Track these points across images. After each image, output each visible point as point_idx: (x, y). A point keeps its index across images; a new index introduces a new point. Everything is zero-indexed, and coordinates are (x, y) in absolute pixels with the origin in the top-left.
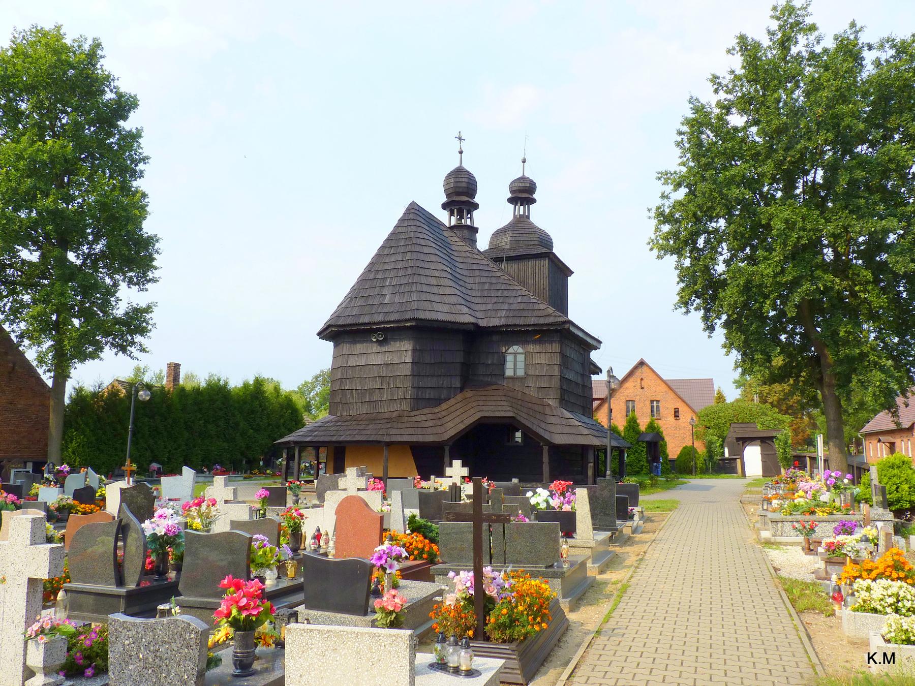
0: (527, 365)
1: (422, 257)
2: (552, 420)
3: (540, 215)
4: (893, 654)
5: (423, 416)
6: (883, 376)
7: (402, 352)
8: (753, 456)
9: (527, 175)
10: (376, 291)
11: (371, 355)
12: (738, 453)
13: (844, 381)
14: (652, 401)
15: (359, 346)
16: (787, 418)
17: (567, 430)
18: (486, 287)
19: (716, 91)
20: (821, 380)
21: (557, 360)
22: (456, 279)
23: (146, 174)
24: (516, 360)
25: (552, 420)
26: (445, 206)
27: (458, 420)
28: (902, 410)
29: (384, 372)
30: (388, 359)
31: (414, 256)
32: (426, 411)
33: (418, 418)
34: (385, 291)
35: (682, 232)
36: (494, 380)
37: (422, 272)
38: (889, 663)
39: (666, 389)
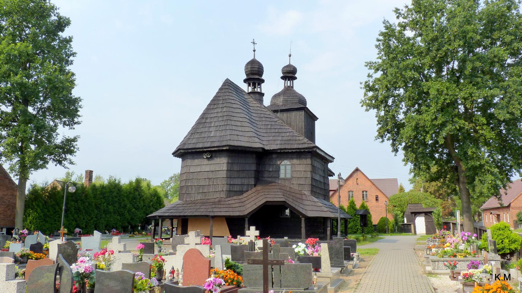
0: (292, 171)
1: (233, 110)
2: (307, 203)
3: (299, 86)
5: (234, 201)
6: (493, 178)
8: (420, 222)
9: (292, 63)
10: (206, 130)
11: (202, 165)
13: (471, 180)
14: (363, 192)
16: (439, 201)
18: (269, 127)
19: (398, 17)
20: (458, 180)
24: (286, 168)
25: (307, 203)
26: (245, 81)
28: (504, 197)
30: (213, 168)
31: (228, 109)
32: (235, 198)
33: (230, 202)
35: (378, 97)
37: (232, 118)
39: (371, 184)
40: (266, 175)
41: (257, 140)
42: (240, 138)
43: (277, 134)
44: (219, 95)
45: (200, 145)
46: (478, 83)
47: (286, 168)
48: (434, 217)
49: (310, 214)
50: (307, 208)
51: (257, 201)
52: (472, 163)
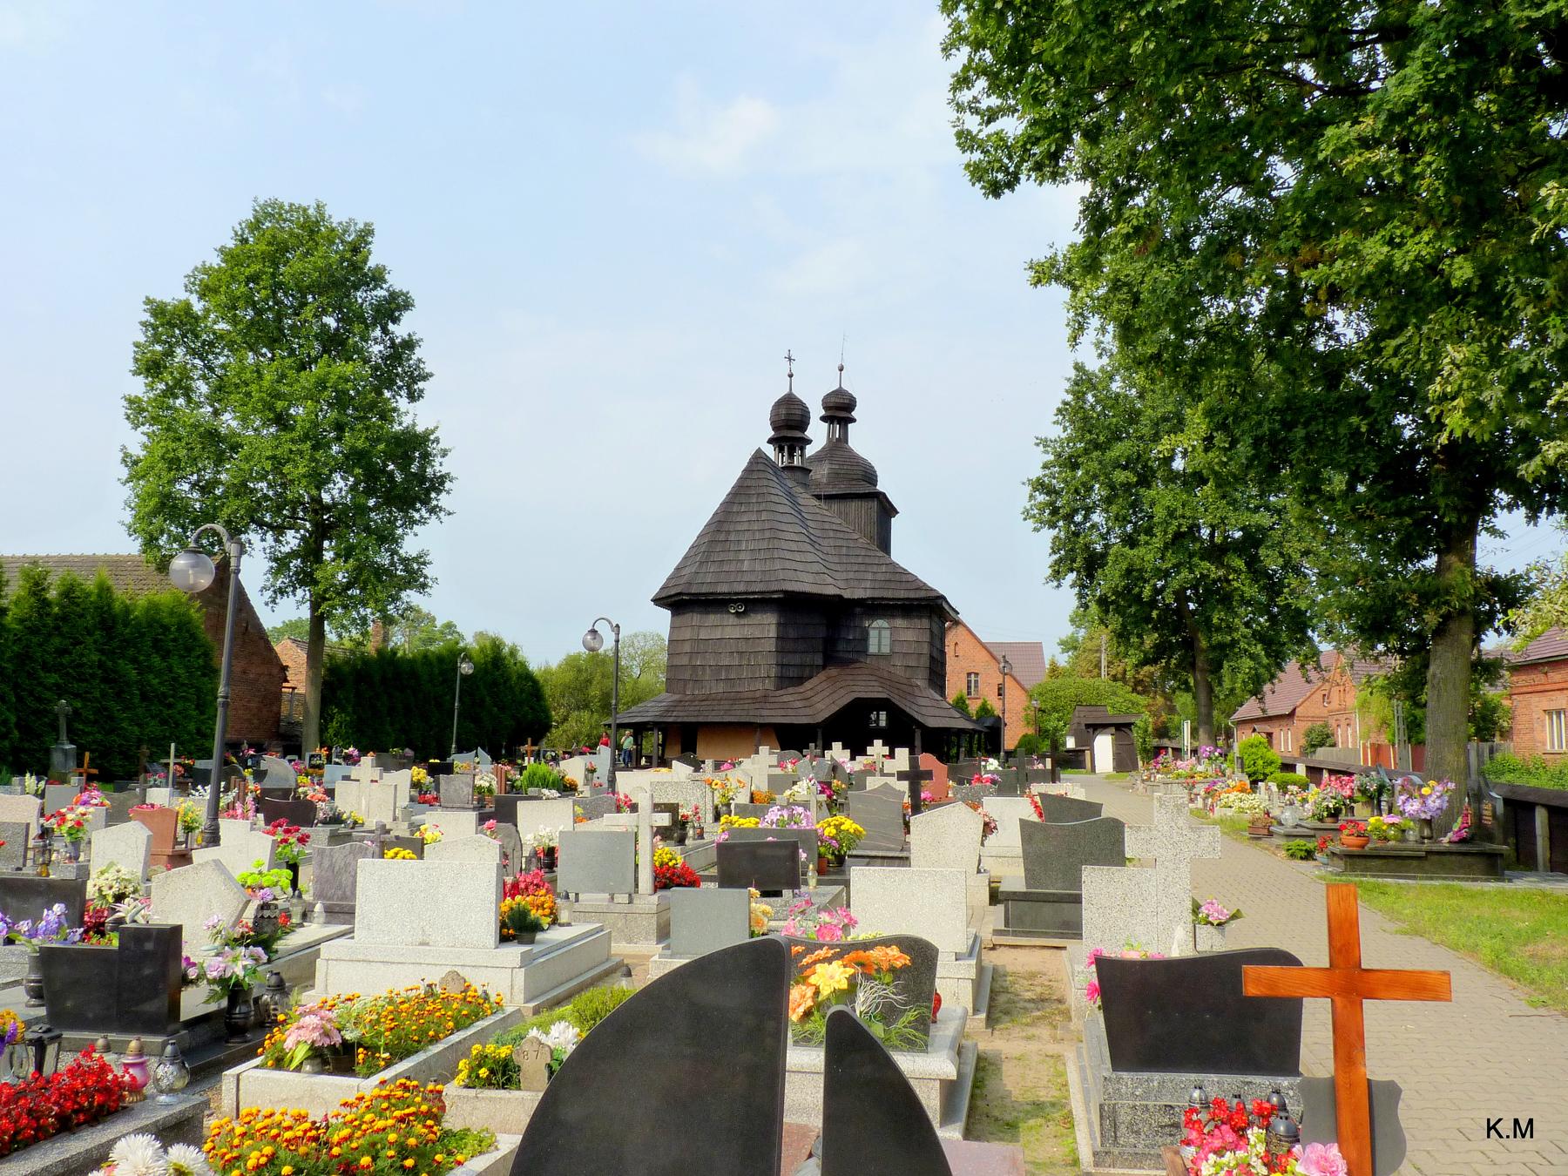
0: (893, 642)
1: (780, 517)
2: (922, 702)
3: (859, 440)
4: (1531, 1121)
5: (790, 696)
6: (1252, 664)
7: (766, 625)
8: (1104, 745)
10: (731, 556)
11: (725, 628)
12: (1086, 742)
13: (1216, 667)
14: (969, 674)
15: (712, 617)
16: (1142, 700)
17: (937, 712)
18: (844, 551)
19: (1100, 356)
20: (1193, 666)
21: (926, 637)
22: (813, 543)
23: (426, 394)
24: (881, 635)
25: (922, 702)
26: (770, 441)
27: (827, 701)
28: (1268, 697)
29: (743, 647)
31: (771, 516)
32: (791, 690)
33: (785, 699)
34: (742, 556)
35: (1058, 504)
36: (856, 656)
37: (781, 535)
38: (1523, 1136)
39: (988, 657)
40: (841, 646)
41: (830, 580)
42: (803, 577)
43: (862, 568)
44: (748, 483)
45: (724, 588)
46: (1235, 501)
47: (881, 635)
48: (1136, 735)
49: (932, 723)
50: (924, 711)
51: (835, 696)
52: (1217, 638)
